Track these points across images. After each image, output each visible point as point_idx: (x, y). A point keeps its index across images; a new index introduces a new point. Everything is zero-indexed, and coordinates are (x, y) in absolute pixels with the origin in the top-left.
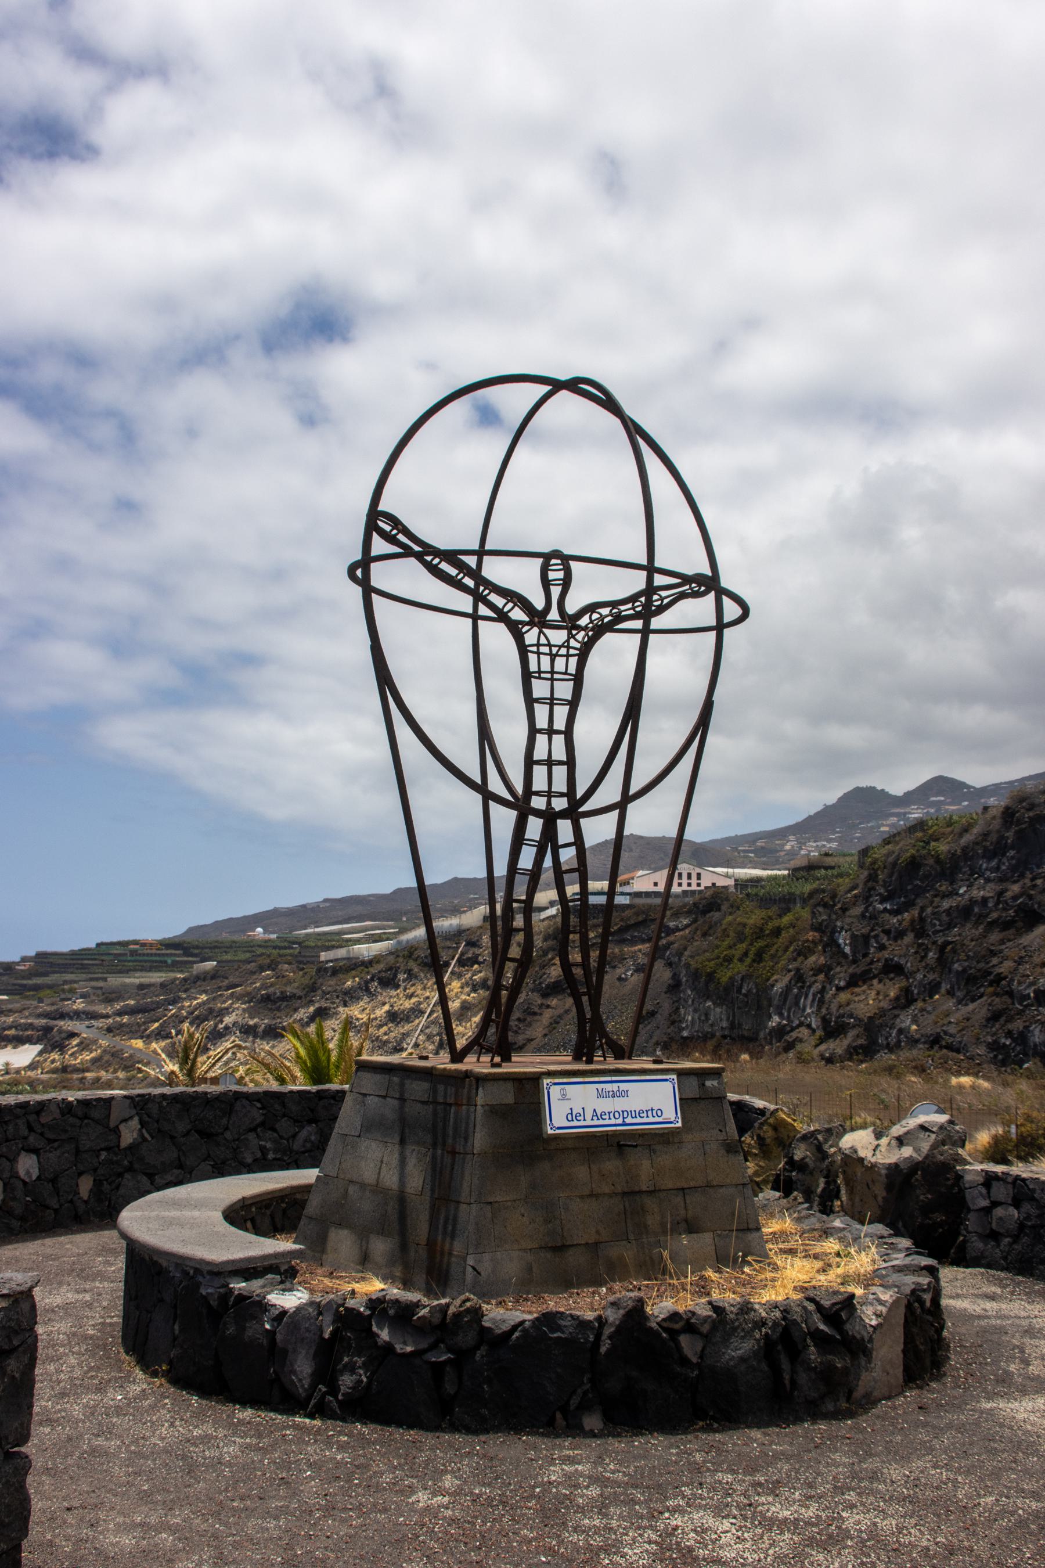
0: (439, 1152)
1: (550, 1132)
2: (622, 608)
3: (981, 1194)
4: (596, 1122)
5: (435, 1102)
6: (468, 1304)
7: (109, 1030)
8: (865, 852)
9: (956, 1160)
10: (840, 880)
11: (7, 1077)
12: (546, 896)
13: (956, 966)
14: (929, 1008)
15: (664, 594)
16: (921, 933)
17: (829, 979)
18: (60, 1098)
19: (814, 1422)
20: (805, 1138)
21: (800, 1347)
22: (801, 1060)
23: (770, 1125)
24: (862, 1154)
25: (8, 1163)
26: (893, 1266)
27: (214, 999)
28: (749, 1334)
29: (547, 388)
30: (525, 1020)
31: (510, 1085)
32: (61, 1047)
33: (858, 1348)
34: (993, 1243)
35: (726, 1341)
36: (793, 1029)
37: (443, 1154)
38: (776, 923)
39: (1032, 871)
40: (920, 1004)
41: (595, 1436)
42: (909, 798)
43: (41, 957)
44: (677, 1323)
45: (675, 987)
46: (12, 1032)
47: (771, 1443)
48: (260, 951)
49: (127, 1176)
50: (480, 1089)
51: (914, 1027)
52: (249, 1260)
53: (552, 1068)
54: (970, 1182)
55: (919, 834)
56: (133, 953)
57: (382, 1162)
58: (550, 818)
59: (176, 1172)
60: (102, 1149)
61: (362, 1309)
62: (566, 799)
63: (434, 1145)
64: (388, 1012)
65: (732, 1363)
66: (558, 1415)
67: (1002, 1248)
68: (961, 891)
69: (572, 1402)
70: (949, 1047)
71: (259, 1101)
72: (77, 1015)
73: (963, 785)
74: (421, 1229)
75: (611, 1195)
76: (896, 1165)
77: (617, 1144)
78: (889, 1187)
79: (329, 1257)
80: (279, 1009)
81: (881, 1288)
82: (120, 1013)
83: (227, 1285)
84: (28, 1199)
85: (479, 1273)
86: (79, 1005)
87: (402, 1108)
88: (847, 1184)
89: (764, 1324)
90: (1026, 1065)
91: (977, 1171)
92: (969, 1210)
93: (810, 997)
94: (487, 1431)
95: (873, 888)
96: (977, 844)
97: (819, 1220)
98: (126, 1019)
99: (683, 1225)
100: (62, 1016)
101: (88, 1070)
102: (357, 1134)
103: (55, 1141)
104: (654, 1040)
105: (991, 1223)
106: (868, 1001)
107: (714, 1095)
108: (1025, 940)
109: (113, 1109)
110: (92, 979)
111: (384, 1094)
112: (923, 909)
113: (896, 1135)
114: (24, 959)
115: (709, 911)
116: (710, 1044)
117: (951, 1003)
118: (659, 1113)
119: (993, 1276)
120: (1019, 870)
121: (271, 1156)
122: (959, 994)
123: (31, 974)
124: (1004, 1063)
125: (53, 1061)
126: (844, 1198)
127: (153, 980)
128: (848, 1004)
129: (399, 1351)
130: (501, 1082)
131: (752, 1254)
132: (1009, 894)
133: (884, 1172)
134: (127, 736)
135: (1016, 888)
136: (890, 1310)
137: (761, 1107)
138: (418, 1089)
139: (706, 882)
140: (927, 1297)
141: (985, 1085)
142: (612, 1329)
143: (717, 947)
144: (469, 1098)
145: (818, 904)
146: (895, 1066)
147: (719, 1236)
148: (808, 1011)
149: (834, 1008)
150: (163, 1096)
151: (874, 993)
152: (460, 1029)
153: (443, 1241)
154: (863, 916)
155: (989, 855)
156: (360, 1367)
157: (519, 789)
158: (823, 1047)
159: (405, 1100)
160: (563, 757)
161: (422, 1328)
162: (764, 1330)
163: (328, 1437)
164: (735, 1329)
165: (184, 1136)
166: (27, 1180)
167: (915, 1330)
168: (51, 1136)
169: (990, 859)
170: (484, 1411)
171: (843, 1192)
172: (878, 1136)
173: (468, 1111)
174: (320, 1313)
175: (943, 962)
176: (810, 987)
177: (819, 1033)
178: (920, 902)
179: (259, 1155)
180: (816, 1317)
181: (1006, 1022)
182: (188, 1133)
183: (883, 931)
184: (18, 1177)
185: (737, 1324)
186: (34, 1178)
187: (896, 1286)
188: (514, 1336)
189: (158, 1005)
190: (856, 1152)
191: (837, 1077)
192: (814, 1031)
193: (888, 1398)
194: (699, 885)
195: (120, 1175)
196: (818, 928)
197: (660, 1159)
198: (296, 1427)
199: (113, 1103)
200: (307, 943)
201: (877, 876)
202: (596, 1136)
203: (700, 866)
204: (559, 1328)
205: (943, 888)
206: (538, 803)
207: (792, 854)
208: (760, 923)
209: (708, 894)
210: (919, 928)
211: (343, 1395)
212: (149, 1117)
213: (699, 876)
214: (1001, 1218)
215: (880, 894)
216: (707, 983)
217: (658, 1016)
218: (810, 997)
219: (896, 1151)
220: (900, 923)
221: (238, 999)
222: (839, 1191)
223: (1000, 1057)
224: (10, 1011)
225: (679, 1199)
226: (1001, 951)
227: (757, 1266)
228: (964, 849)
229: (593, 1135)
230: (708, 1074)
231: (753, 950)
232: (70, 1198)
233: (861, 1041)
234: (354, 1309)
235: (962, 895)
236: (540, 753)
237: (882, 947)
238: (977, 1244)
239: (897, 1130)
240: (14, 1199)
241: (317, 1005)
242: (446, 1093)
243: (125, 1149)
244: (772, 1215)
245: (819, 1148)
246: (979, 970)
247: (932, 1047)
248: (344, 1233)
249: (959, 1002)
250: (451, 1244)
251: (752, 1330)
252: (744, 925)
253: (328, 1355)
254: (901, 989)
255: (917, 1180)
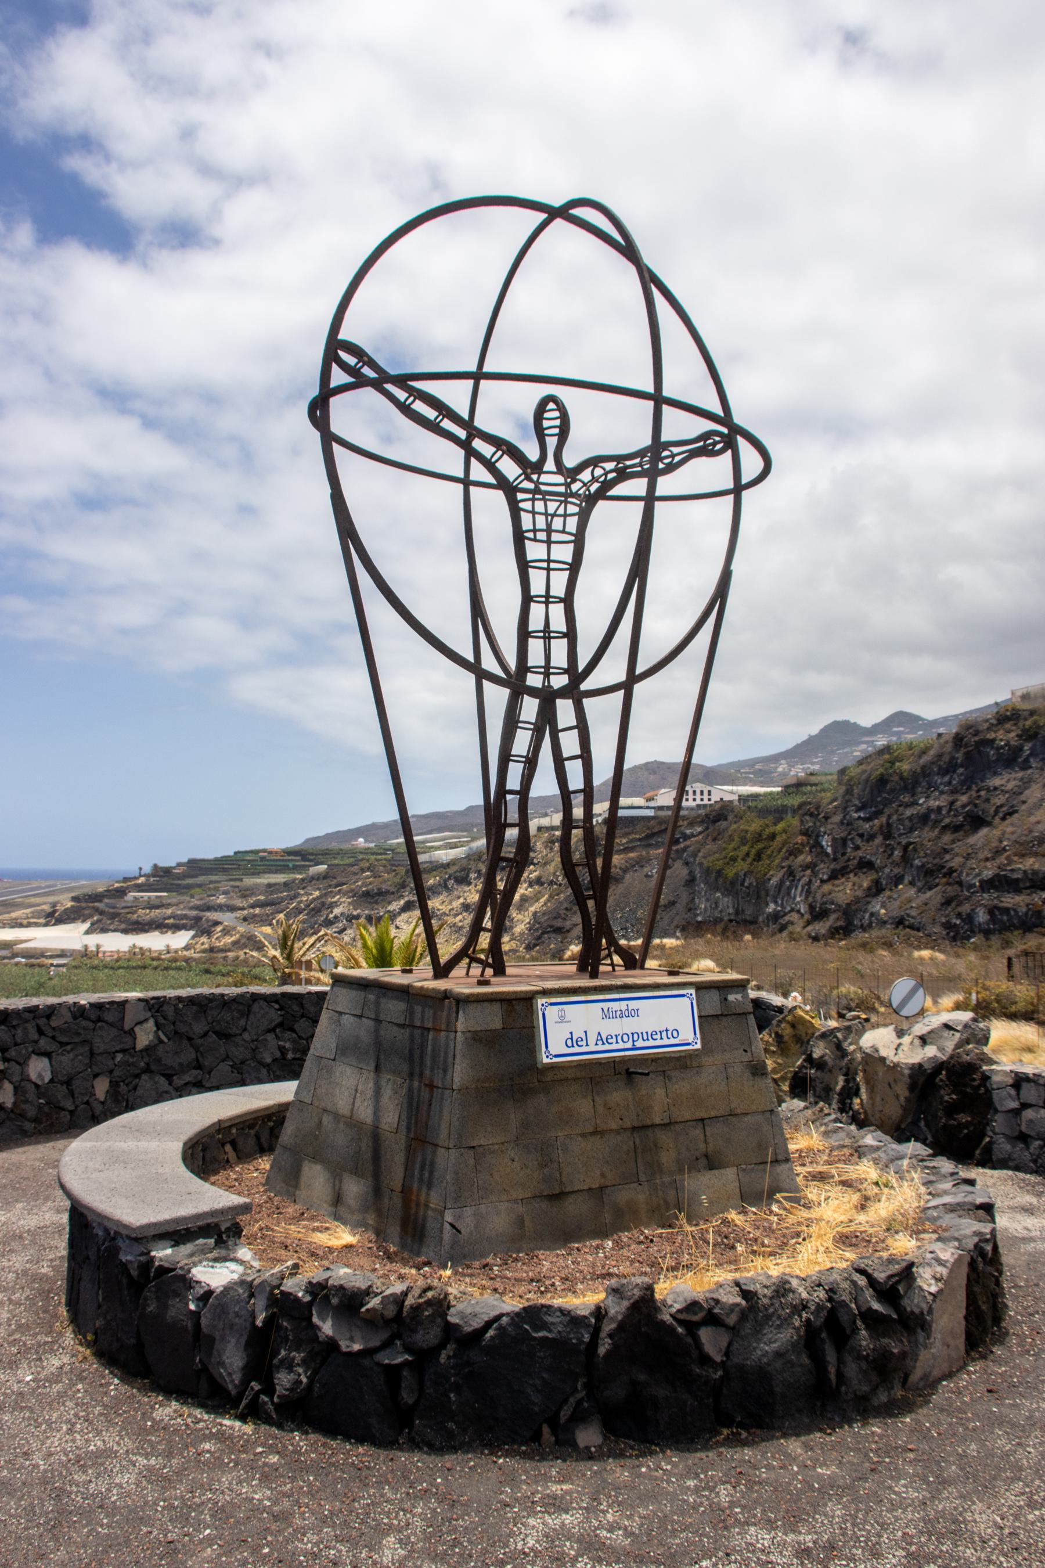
0: (416, 1084)
1: (546, 1060)
2: (628, 463)
3: (1010, 1095)
5: (412, 1026)
6: (430, 1294)
7: (245, 919)
8: (843, 771)
9: (982, 1060)
10: (823, 794)
11: (168, 956)
12: (545, 785)
13: (917, 862)
14: (895, 896)
15: (675, 450)
16: (888, 836)
17: (815, 874)
18: (71, 1001)
19: (865, 1424)
20: (824, 1036)
21: (848, 1332)
22: (793, 938)
23: (788, 1022)
24: (883, 1053)
25: (18, 1067)
26: (944, 1205)
27: (326, 895)
28: (786, 1321)
29: (543, 216)
30: (571, 909)
31: (497, 1007)
32: (208, 933)
33: (914, 1324)
34: (1022, 1145)
35: (757, 1332)
36: (785, 914)
37: (420, 1086)
38: (771, 829)
39: (976, 784)
40: (887, 893)
41: (591, 1458)
42: (876, 729)
43: (192, 862)
44: (696, 1314)
45: (691, 881)
46: (171, 921)
47: (816, 1462)
48: (361, 857)
49: (144, 1077)
50: (461, 1013)
51: (883, 911)
52: (177, 1221)
53: (549, 985)
54: (999, 1082)
55: (887, 756)
56: (263, 859)
57: (356, 1090)
58: (548, 698)
59: (195, 1072)
60: (117, 1052)
61: (300, 1294)
62: (566, 676)
63: (411, 1075)
64: (463, 904)
65: (765, 1360)
66: (546, 1429)
67: (1031, 1151)
68: (921, 802)
69: (562, 1413)
70: (911, 927)
71: (276, 1002)
72: (220, 908)
73: (918, 718)
74: (395, 1174)
75: (617, 1132)
76: (920, 1065)
77: (627, 1071)
78: (912, 1088)
79: (302, 1194)
80: (376, 902)
81: (939, 1244)
82: (253, 906)
83: (148, 1253)
84: (41, 1101)
85: (459, 1231)
86: (222, 899)
87: (377, 1030)
88: (867, 1082)
89: (805, 1307)
90: (972, 940)
91: (1005, 1072)
92: (996, 1111)
93: (800, 888)
94: (454, 1449)
95: (850, 801)
96: (933, 763)
97: (849, 1135)
98: (257, 911)
99: (703, 1161)
100: (209, 908)
101: (229, 950)
102: (332, 1057)
103: (68, 1044)
104: (674, 924)
105: (1020, 1125)
106: (845, 891)
107: (738, 1011)
108: (972, 840)
109: (127, 1012)
110: (231, 880)
111: (359, 1013)
112: (889, 817)
113: (919, 1034)
114: (179, 865)
115: (718, 821)
116: (719, 928)
117: (912, 892)
119: (1024, 1180)
120: (968, 783)
121: (290, 1056)
122: (919, 884)
123: (184, 876)
124: (954, 939)
125: (203, 944)
126: (864, 1097)
127: (278, 881)
128: (830, 893)
129: (344, 1349)
130: (486, 1004)
131: (780, 1191)
132: (959, 803)
133: (907, 1072)
134: (253, 690)
135: (964, 799)
136: (951, 1271)
137: (779, 1004)
138: (394, 1009)
139: (715, 798)
140: (989, 1248)
141: (940, 956)
142: (613, 1326)
143: (725, 849)
144: (448, 1024)
145: (806, 814)
146: (868, 943)
147: (744, 1170)
148: (798, 899)
149: (818, 897)
150: (179, 999)
151: (850, 884)
152: (520, 917)
153: (419, 1190)
154: (842, 823)
155: (945, 771)
156: (298, 1365)
157: (512, 663)
158: (809, 928)
159: (381, 1022)
160: (564, 629)
161: (373, 1322)
162: (804, 1315)
163: (255, 1454)
164: (768, 1317)
165: (201, 1037)
166: (40, 1083)
167: (977, 1289)
168: (64, 1039)
169: (944, 775)
170: (451, 1425)
171: (863, 1090)
172: (900, 1033)
173: (447, 1037)
174: (252, 1295)
175: (906, 859)
176: (799, 880)
177: (807, 916)
178: (887, 811)
179: (278, 1055)
180: (868, 1293)
181: (957, 905)
182: (205, 1034)
183: (858, 835)
184: (30, 1081)
185: (771, 1310)
186: (47, 1080)
187: (956, 1239)
188: (488, 1335)
189: (283, 900)
190: (877, 1051)
191: (822, 952)
192: (802, 915)
193: (949, 1375)
194: (709, 800)
195: (138, 1076)
196: (805, 833)
197: (676, 1086)
198: (221, 1437)
199: (127, 1006)
200: (398, 850)
201: (853, 790)
202: (601, 1064)
203: (711, 785)
204: (545, 1326)
205: (906, 799)
206: (534, 680)
207: (784, 774)
208: (758, 830)
209: (717, 807)
210: (887, 833)
211: (279, 1396)
212: (165, 1019)
213: (709, 793)
214: (1031, 1121)
215: (855, 805)
216: (716, 879)
217: (677, 905)
218: (800, 888)
219: (920, 1050)
220: (872, 827)
221: (344, 895)
222: (858, 1089)
223: (952, 934)
224: (169, 904)
225: (698, 1132)
226: (952, 850)
227: (787, 1205)
228: (923, 768)
229: (598, 1063)
230: (732, 987)
231: (753, 851)
232: (85, 1100)
233: (839, 924)
234: (290, 1294)
235: (921, 805)
236: (536, 622)
237: (857, 848)
238: (1003, 1147)
239: (920, 1029)
240: (26, 1101)
241: (406, 899)
242: (423, 1017)
243: (141, 1051)
244: (797, 1129)
245: (839, 1046)
246: (935, 865)
247: (897, 927)
248: (318, 1168)
249: (919, 890)
250: (428, 1194)
251: (791, 1316)
252: (747, 831)
253: (262, 1345)
254: (872, 881)
255: (941, 1080)
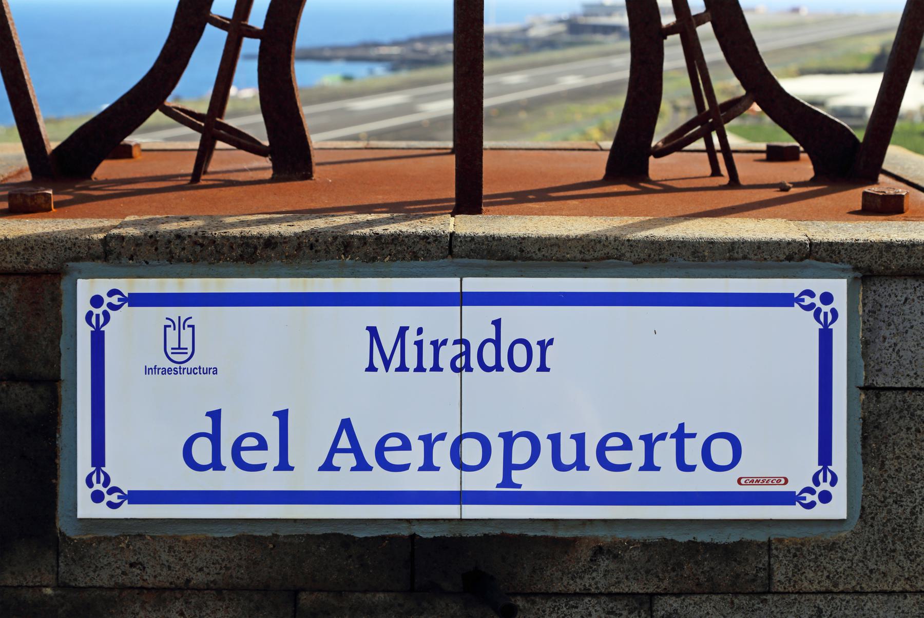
4: (346, 479)
118: (722, 452)
229: (337, 540)
